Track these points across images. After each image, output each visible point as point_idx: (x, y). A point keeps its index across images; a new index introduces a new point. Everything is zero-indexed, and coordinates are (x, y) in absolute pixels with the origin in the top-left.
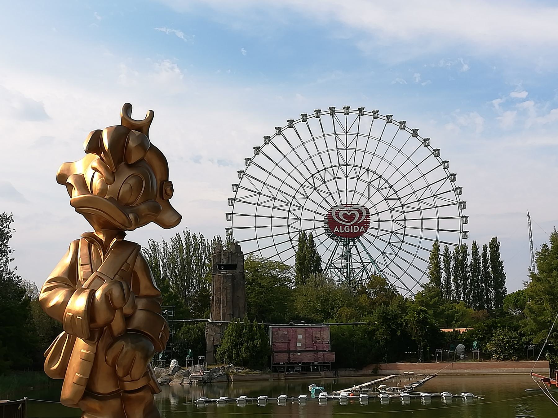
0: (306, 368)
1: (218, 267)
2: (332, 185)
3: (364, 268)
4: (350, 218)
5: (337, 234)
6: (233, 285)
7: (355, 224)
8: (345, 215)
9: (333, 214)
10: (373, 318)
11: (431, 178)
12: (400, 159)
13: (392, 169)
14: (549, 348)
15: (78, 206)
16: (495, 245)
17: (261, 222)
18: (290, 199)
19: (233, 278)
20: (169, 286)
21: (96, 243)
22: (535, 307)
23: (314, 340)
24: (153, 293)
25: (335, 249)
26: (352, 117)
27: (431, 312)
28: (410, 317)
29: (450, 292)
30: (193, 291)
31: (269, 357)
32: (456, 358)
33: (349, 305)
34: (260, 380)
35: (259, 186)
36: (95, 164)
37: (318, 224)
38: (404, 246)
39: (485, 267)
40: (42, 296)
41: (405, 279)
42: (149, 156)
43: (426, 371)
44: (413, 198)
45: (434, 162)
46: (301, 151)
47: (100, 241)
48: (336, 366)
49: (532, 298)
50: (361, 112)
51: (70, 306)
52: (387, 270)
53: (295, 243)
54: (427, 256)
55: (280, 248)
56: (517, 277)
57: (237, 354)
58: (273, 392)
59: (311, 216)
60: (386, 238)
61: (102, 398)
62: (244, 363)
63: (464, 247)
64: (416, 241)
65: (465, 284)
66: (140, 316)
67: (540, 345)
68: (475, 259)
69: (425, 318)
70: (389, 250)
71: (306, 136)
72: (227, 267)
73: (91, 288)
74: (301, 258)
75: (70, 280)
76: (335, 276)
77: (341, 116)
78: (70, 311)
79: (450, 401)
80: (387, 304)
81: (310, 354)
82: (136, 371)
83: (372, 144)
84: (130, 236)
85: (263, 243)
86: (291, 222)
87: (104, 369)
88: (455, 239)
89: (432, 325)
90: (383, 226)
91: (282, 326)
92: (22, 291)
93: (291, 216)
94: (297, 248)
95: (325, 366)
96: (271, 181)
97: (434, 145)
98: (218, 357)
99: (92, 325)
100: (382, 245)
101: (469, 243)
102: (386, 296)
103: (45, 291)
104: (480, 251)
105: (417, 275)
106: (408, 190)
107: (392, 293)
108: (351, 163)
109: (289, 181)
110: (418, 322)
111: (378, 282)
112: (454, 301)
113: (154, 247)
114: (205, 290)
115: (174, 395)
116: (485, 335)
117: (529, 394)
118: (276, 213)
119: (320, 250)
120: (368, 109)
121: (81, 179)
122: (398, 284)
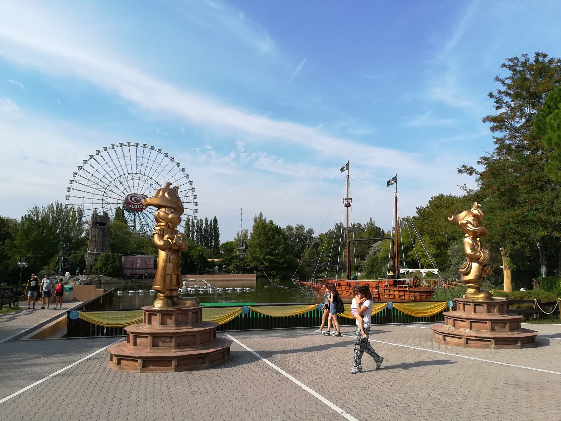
4: (138, 201)
5: (130, 209)
6: (103, 235)
9: (129, 198)
16: (215, 220)
19: (104, 230)
23: (146, 263)
26: (147, 150)
32: (214, 273)
34: (117, 283)
35: (89, 176)
39: (211, 230)
50: (152, 149)
57: (106, 270)
62: (109, 275)
65: (201, 237)
68: (206, 226)
72: (100, 224)
96: (97, 174)
104: (209, 223)
110: (198, 256)
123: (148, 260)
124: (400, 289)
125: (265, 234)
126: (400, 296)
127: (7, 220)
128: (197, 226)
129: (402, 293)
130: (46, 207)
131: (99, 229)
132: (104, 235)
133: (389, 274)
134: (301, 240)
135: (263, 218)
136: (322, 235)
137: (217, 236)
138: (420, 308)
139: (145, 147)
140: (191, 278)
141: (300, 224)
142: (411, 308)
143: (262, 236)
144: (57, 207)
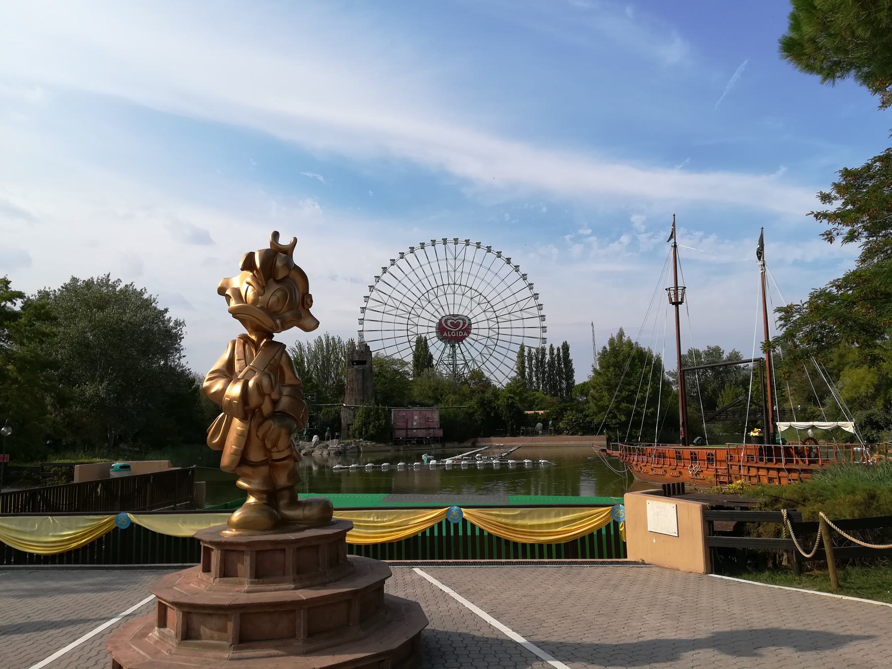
0: (420, 441)
1: (352, 362)
2: (442, 300)
3: (466, 364)
4: (456, 325)
6: (363, 378)
10: (473, 403)
11: (519, 297)
12: (496, 281)
13: (489, 289)
14: (606, 426)
15: (235, 313)
16: (566, 347)
17: (386, 326)
18: (410, 309)
19: (363, 371)
20: (312, 378)
21: (250, 342)
22: (596, 395)
23: (427, 419)
24: (296, 383)
25: (444, 349)
26: (460, 246)
27: (517, 398)
28: (501, 402)
29: (531, 383)
30: (331, 382)
31: (391, 434)
32: (535, 433)
33: (454, 393)
35: (386, 298)
36: (249, 280)
37: (431, 329)
38: (497, 349)
39: (559, 364)
40: (206, 384)
41: (498, 374)
42: (293, 274)
43: (513, 444)
44: (505, 311)
45: (522, 284)
46: (419, 272)
47: (253, 341)
48: (443, 440)
49: (594, 388)
51: (227, 392)
52: (483, 366)
53: (413, 344)
54: (515, 356)
55: (401, 347)
56: (583, 371)
57: (366, 431)
58: (394, 461)
59: (426, 323)
60: (484, 341)
61: (254, 465)
62: (371, 438)
63: (543, 349)
64: (506, 345)
65: (543, 377)
66: (285, 402)
67: (599, 424)
68: (552, 358)
69: (513, 403)
70: (485, 351)
71: (423, 260)
72: (359, 363)
73: (246, 378)
74: (417, 357)
75: (228, 372)
76: (444, 370)
77: (451, 246)
78: (228, 396)
79: (531, 467)
80: (483, 392)
81: (423, 431)
82: (282, 444)
83: (475, 268)
84: (278, 337)
85: (387, 343)
86: (409, 327)
87: (256, 442)
88: (536, 344)
89: (518, 408)
90: (482, 332)
91: (402, 409)
92: (193, 381)
93: (410, 322)
94: (414, 348)
95: (435, 440)
96: (395, 294)
97: (522, 270)
98: (350, 433)
99: (246, 408)
100: (480, 347)
101: (547, 346)
102: (483, 386)
103: (209, 380)
104: (555, 352)
105: (507, 371)
106: (502, 305)
107: (488, 383)
108: (458, 282)
109: (409, 295)
111: (477, 375)
112: (535, 390)
113: (300, 346)
114: (341, 381)
115: (315, 463)
116: (559, 416)
117: (589, 461)
118: (399, 320)
119: (432, 350)
120: (473, 241)
121: (237, 292)
122: (492, 377)
123: (429, 415)
124: (770, 465)
125: (618, 366)
126: (771, 480)
128: (537, 358)
129: (773, 474)
131: (357, 370)
132: (364, 379)
134: (717, 374)
137: (570, 372)
138: (535, 522)
139: (456, 244)
140: (498, 442)
141: (713, 345)
142: (508, 521)
143: (611, 369)
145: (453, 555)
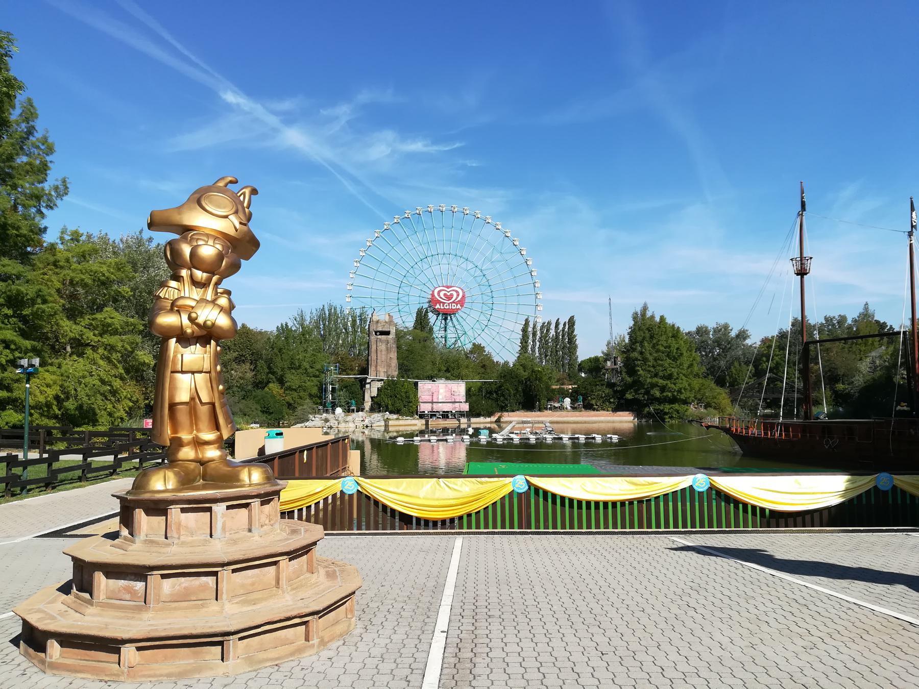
7: (453, 302)
8: (445, 295)
16: (571, 322)
32: (561, 408)
68: (556, 332)
104: (561, 327)
127: (260, 333)
128: (542, 332)
130: (314, 311)
133: (899, 408)
135: (649, 314)
136: (766, 342)
144: (330, 310)
145: (364, 527)
